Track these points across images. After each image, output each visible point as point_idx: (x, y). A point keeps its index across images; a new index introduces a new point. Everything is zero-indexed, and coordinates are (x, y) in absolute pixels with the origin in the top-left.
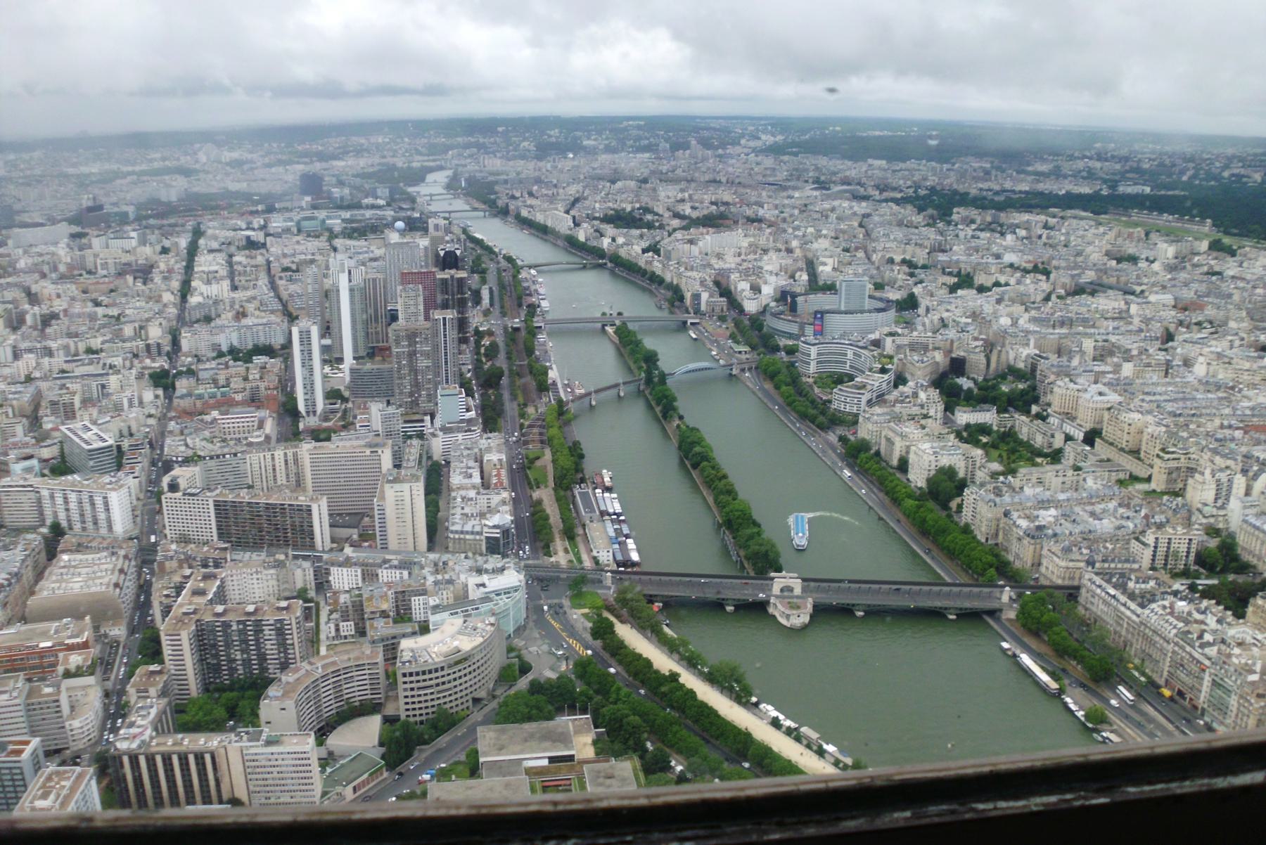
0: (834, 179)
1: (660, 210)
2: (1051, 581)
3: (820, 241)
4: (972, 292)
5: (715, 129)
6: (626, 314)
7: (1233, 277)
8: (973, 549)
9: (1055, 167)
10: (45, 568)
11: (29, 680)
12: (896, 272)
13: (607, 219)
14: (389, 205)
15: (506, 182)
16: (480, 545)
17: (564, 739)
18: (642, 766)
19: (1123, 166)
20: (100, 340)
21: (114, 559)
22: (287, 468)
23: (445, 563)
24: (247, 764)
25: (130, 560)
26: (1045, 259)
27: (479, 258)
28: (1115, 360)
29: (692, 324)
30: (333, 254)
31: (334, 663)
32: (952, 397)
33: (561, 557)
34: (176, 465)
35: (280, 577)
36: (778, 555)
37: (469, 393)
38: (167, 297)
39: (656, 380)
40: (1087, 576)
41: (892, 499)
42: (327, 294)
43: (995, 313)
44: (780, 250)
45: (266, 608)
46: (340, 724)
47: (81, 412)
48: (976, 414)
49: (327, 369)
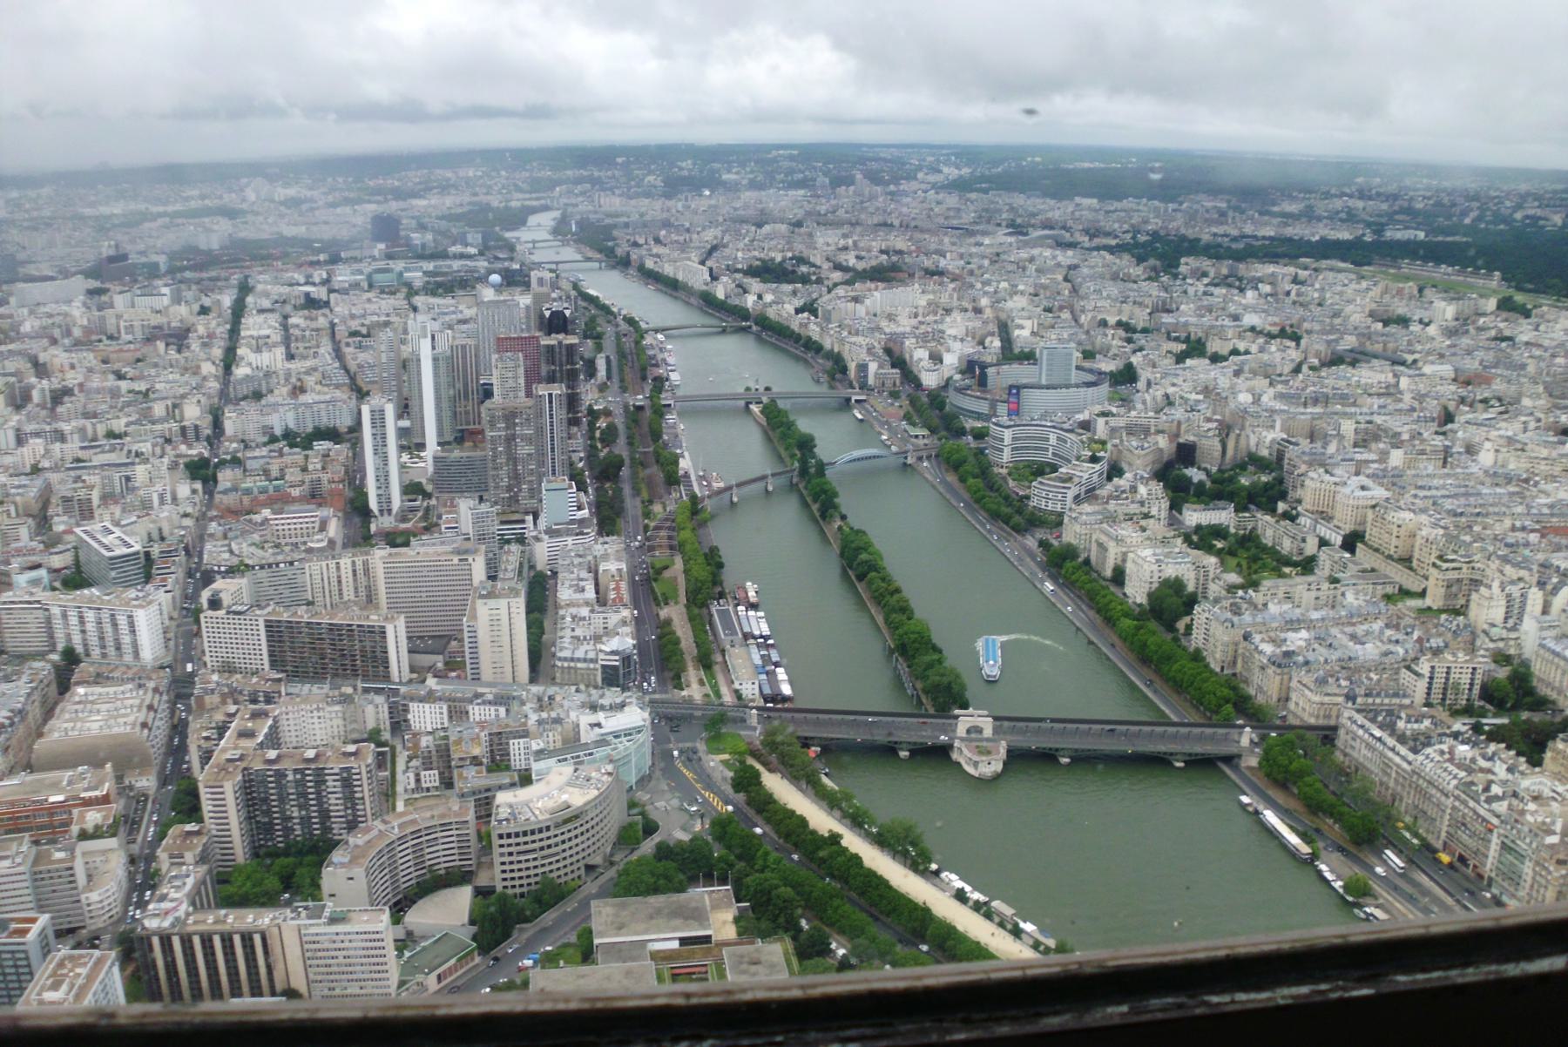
0: (1033, 221)
1: (817, 260)
2: (1302, 720)
3: (1015, 298)
4: (1204, 362)
5: (885, 160)
6: (775, 389)
7: (1527, 343)
9: (1307, 207)
10: (56, 704)
11: (36, 843)
12: (1110, 337)
13: (752, 272)
14: (481, 253)
15: (627, 225)
16: (595, 675)
17: (699, 916)
18: (795, 949)
19: (1391, 206)
20: (124, 421)
21: (141, 692)
22: (355, 580)
23: (551, 698)
24: (306, 946)
25: (161, 694)
26: (1294, 321)
27: (593, 319)
29: (857, 401)
30: (412, 315)
31: (414, 822)
32: (1180, 492)
33: (694, 690)
34: (218, 577)
35: (347, 715)
36: (963, 687)
37: (581, 487)
38: (207, 368)
39: (812, 470)
40: (1346, 714)
41: (1105, 618)
42: (404, 365)
43: (1232, 387)
44: (966, 310)
46: (421, 898)
47: (100, 511)
48: (1209, 513)
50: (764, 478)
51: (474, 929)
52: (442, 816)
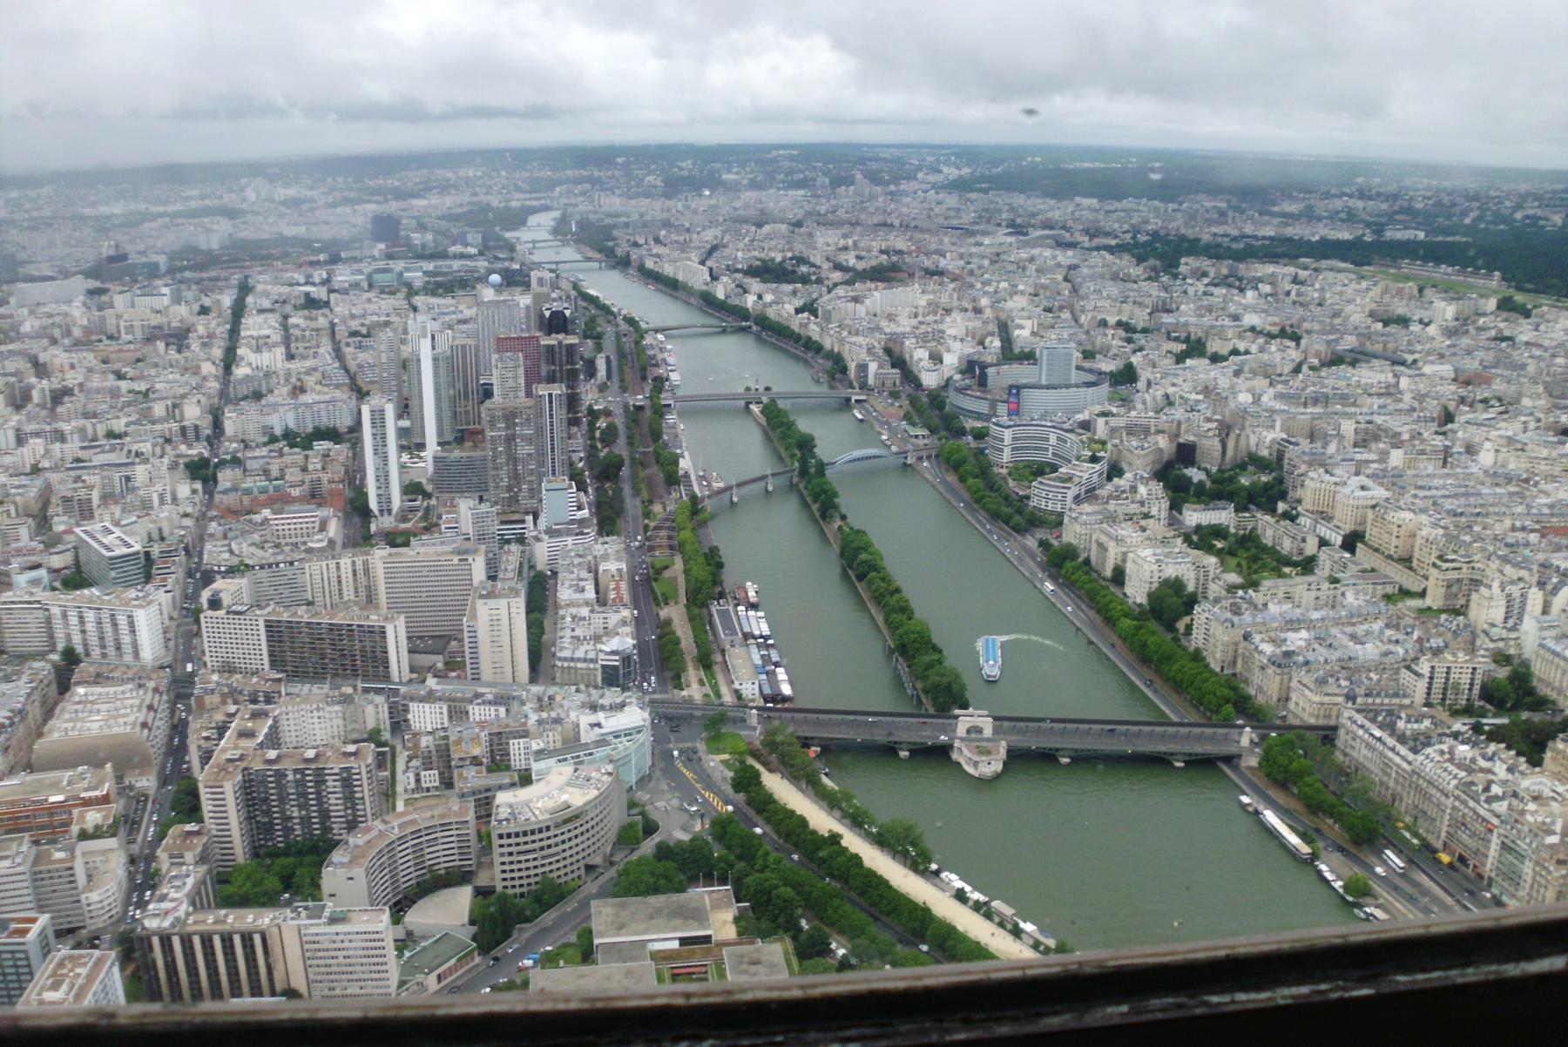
0: (1033, 221)
1: (817, 260)
2: (1302, 720)
3: (1015, 298)
4: (1204, 362)
5: (885, 160)
6: (775, 389)
7: (1527, 343)
8: (1205, 681)
9: (1307, 207)
10: (56, 704)
11: (36, 843)
12: (1110, 337)
13: (752, 272)
14: (481, 253)
15: (627, 225)
16: (595, 675)
17: (699, 916)
18: (795, 949)
19: (1391, 206)
20: (124, 421)
21: (141, 692)
22: (355, 580)
23: (551, 698)
24: (306, 946)
25: (161, 694)
26: (1294, 321)
27: (593, 319)
28: (1381, 446)
29: (857, 401)
30: (412, 315)
31: (414, 822)
32: (1180, 492)
33: (694, 690)
34: (218, 577)
35: (347, 715)
36: (963, 687)
37: (581, 487)
38: (207, 368)
39: (812, 470)
40: (1346, 714)
41: (1105, 618)
42: (404, 365)
43: (1232, 387)
44: (966, 310)
45: (329, 753)
46: (421, 898)
47: (100, 511)
48: (1209, 513)
49: (405, 457)
50: (764, 478)
51: (474, 929)
52: (442, 816)
